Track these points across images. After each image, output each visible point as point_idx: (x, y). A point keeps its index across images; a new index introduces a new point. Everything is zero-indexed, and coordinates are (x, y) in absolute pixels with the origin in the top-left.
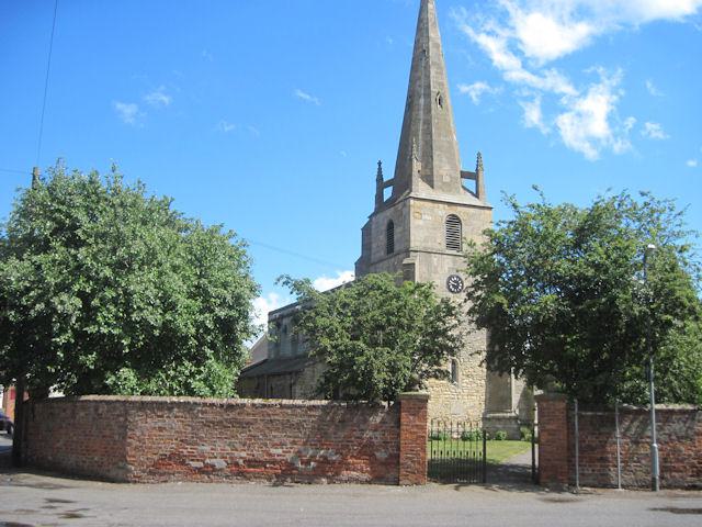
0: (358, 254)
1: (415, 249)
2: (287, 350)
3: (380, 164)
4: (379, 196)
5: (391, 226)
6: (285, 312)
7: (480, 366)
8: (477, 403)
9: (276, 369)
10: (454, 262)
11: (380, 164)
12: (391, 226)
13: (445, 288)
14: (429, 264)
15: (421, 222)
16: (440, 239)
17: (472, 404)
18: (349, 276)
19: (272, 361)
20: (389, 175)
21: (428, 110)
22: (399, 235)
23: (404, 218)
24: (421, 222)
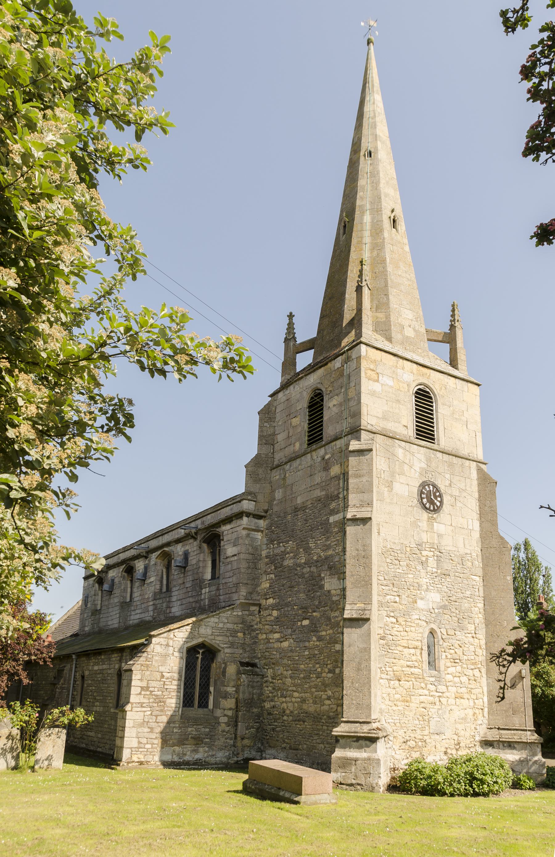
0: (251, 449)
1: (369, 428)
2: (113, 619)
3: (291, 316)
4: (289, 363)
5: (316, 404)
6: (153, 544)
7: (38, 586)
8: (470, 712)
9: (86, 646)
10: (429, 460)
11: (291, 316)
12: (316, 404)
13: (416, 501)
14: (391, 456)
15: (377, 387)
16: (405, 420)
17: (462, 714)
18: (351, 443)
19: (89, 634)
20: (307, 330)
21: (377, 231)
22: (335, 410)
23: (349, 382)
24: (377, 387)
